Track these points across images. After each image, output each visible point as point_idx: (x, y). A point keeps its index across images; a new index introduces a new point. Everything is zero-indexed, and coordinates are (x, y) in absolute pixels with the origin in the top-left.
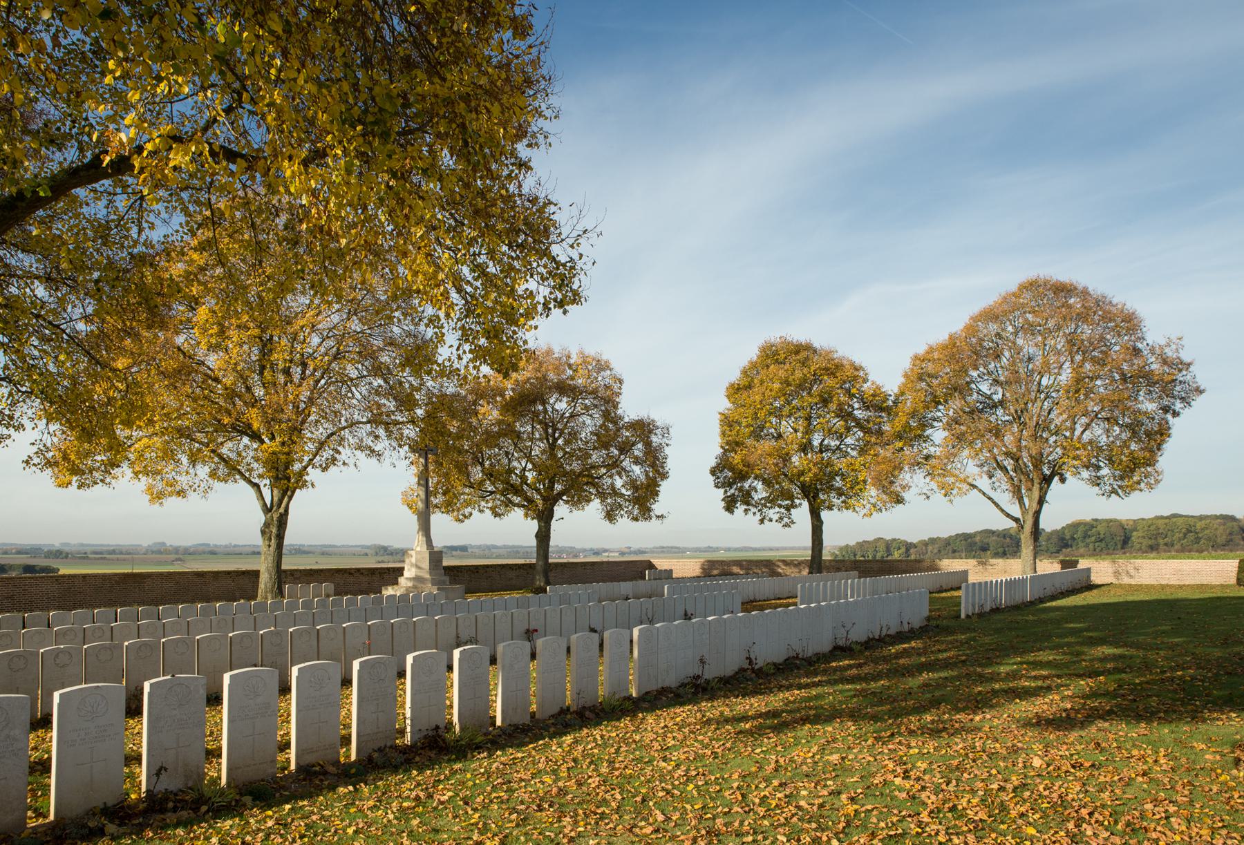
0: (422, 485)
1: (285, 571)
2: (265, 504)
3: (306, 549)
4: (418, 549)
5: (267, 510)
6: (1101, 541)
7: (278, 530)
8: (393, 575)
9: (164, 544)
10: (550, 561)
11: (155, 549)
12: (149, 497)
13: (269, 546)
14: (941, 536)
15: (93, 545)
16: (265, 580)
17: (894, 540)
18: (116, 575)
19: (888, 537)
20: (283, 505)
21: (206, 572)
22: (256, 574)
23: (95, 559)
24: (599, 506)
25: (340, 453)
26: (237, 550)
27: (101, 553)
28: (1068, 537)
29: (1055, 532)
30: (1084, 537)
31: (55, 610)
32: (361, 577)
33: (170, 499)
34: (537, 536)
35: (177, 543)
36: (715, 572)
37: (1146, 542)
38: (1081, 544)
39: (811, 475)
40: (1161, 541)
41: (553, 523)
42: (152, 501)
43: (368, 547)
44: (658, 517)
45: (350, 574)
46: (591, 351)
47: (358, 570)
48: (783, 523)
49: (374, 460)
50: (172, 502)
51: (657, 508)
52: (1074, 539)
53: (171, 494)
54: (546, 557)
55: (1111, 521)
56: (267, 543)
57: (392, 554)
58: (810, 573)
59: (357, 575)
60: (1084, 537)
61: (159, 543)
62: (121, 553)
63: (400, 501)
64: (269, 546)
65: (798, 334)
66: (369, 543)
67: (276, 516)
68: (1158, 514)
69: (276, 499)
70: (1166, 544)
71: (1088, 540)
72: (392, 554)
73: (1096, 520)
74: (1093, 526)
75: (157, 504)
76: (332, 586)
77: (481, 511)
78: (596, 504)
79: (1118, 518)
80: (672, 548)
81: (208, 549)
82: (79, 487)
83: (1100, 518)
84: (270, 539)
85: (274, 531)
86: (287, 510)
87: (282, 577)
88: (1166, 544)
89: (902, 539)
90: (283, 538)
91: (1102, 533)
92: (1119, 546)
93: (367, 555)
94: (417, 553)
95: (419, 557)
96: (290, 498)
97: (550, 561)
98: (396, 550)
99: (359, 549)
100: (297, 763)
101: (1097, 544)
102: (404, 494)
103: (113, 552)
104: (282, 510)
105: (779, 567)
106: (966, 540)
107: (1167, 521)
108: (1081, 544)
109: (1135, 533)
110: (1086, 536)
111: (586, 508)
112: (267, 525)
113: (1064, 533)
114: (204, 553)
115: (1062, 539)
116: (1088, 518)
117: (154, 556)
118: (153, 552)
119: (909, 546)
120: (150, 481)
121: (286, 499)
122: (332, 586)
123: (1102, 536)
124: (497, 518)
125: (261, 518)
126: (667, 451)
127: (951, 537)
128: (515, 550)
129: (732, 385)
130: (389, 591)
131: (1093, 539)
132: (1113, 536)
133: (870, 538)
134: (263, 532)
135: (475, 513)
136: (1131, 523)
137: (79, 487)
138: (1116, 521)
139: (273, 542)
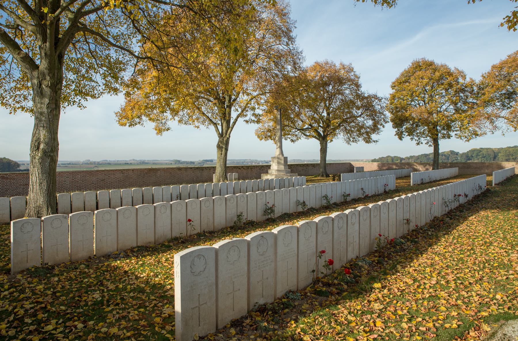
1: (228, 167)
3: (146, 162)
6: (484, 157)
8: (265, 168)
9: (89, 160)
10: (327, 162)
11: (86, 162)
13: (221, 154)
14: (415, 155)
15: (62, 161)
16: (219, 170)
17: (395, 157)
18: (146, 169)
19: (392, 155)
21: (182, 168)
22: (214, 168)
23: (63, 167)
26: (119, 162)
27: (65, 164)
28: (470, 156)
29: (463, 154)
30: (477, 156)
31: (173, 185)
32: (244, 170)
35: (94, 160)
36: (385, 168)
37: (504, 158)
38: (475, 159)
39: (443, 122)
40: (511, 157)
42: (157, 134)
43: (172, 161)
44: (374, 141)
45: (239, 168)
46: (346, 63)
47: (243, 167)
48: (429, 144)
50: (165, 133)
52: (472, 157)
53: (164, 130)
54: (325, 160)
55: (488, 149)
56: (220, 152)
57: (182, 163)
58: (433, 169)
59: (242, 169)
60: (477, 156)
61: (87, 160)
62: (73, 164)
64: (221, 154)
65: (429, 58)
66: (172, 159)
67: (225, 139)
68: (509, 146)
69: (224, 131)
70: (513, 159)
71: (478, 157)
72: (182, 163)
73: (482, 148)
74: (480, 151)
76: (237, 174)
77: (286, 139)
79: (491, 147)
80: (298, 160)
81: (107, 162)
82: (129, 126)
83: (483, 147)
86: (230, 136)
87: (227, 169)
88: (513, 159)
89: (398, 156)
91: (485, 154)
92: (492, 160)
93: (172, 164)
97: (327, 162)
98: (183, 162)
99: (168, 161)
101: (482, 159)
103: (70, 164)
105: (414, 165)
106: (426, 157)
107: (513, 149)
108: (475, 159)
109: (500, 154)
110: (477, 155)
113: (468, 154)
114: (106, 164)
115: (467, 156)
116: (478, 148)
117: (86, 165)
118: (85, 164)
119: (402, 159)
121: (229, 131)
122: (237, 174)
123: (484, 155)
127: (419, 155)
129: (494, 65)
130: (265, 177)
131: (481, 156)
132: (489, 155)
133: (385, 156)
136: (497, 150)
137: (129, 126)
138: (490, 149)
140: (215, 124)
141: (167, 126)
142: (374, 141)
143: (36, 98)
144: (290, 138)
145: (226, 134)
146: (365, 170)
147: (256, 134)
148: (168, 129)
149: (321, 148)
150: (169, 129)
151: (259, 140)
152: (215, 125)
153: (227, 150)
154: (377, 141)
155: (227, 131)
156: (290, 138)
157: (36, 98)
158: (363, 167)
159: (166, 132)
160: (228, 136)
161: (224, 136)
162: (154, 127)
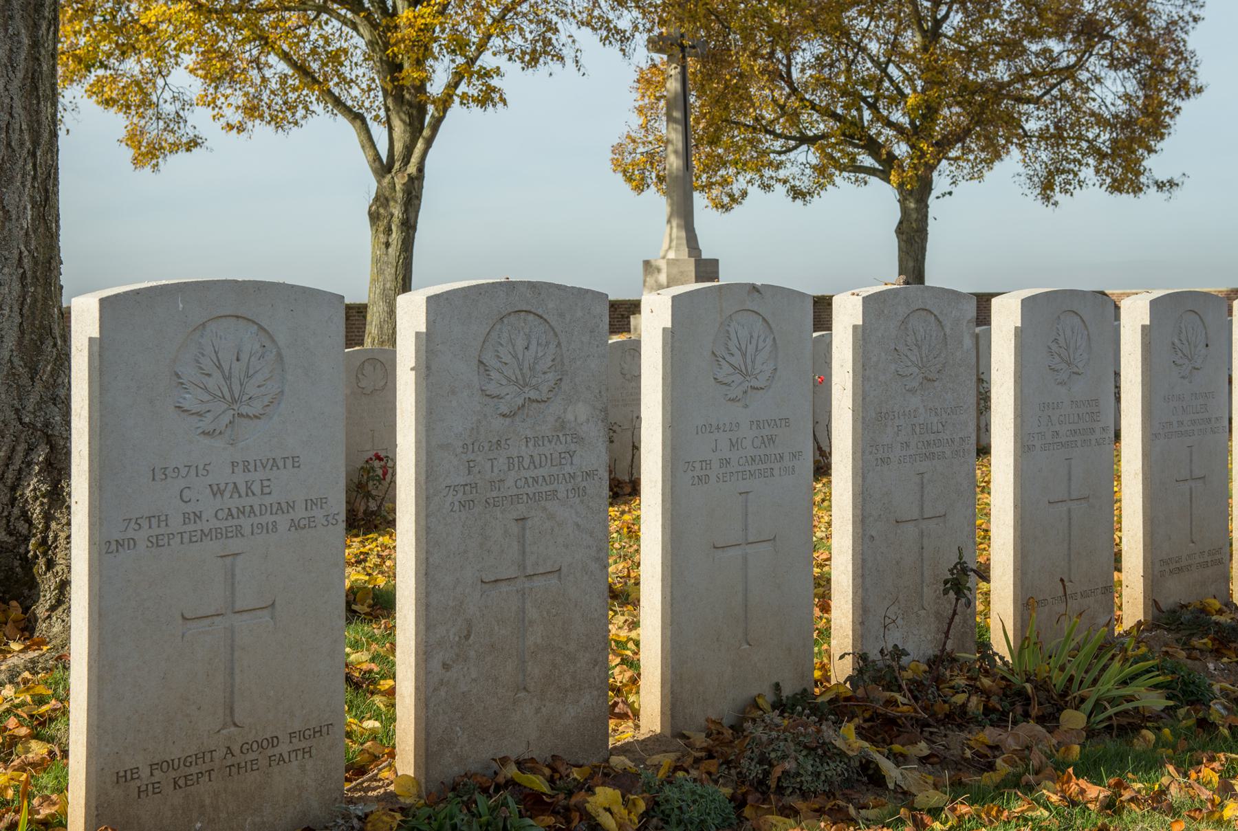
0: (675, 121)
2: (377, 157)
4: (671, 255)
5: (383, 168)
7: (406, 211)
10: (704, 257)
12: (130, 153)
13: (387, 245)
20: (414, 159)
24: (1020, 168)
25: (556, 31)
33: (172, 158)
34: (900, 231)
41: (932, 201)
42: (137, 162)
44: (1160, 186)
49: (614, 50)
50: (175, 163)
51: (1156, 165)
53: (175, 147)
56: (383, 238)
63: (609, 166)
64: (387, 245)
67: (400, 182)
69: (398, 147)
75: (148, 169)
77: (766, 187)
78: (1013, 160)
84: (389, 231)
85: (397, 211)
86: (421, 169)
90: (414, 228)
94: (671, 263)
95: (675, 271)
96: (429, 142)
100: (1152, 601)
102: (618, 149)
104: (412, 169)
111: (987, 174)
112: (382, 200)
120: (135, 120)
121: (420, 145)
124: (799, 202)
125: (369, 185)
126: (1195, 40)
128: (414, 377)
134: (374, 217)
135: (754, 191)
139: (395, 237)
140: (357, 118)
141: (187, 132)
142: (1160, 186)
143: (950, 155)
144: (785, 182)
145: (406, 160)
146: (1148, 323)
147: (618, 165)
148: (193, 144)
149: (901, 223)
150: (196, 144)
151: (627, 188)
152: (358, 122)
153: (409, 226)
154: (1172, 184)
155: (409, 150)
156: (785, 182)
157: (950, 155)
158: (717, 261)
159: (182, 154)
160: (412, 169)
161: (397, 166)
162: (123, 134)
